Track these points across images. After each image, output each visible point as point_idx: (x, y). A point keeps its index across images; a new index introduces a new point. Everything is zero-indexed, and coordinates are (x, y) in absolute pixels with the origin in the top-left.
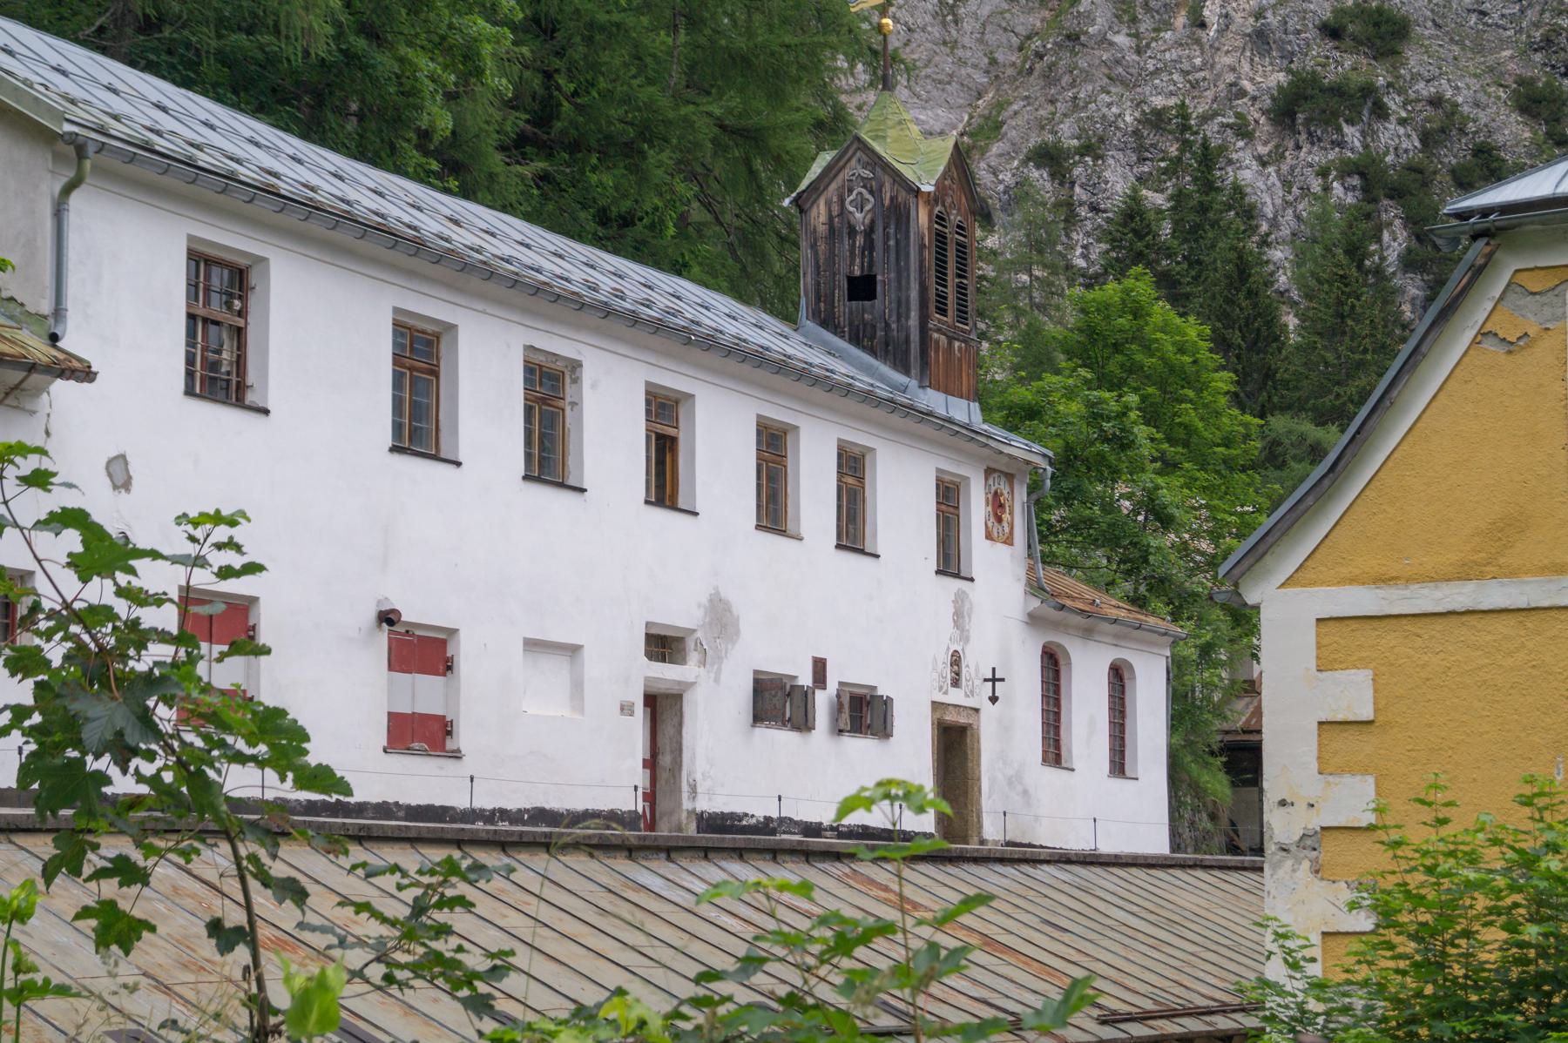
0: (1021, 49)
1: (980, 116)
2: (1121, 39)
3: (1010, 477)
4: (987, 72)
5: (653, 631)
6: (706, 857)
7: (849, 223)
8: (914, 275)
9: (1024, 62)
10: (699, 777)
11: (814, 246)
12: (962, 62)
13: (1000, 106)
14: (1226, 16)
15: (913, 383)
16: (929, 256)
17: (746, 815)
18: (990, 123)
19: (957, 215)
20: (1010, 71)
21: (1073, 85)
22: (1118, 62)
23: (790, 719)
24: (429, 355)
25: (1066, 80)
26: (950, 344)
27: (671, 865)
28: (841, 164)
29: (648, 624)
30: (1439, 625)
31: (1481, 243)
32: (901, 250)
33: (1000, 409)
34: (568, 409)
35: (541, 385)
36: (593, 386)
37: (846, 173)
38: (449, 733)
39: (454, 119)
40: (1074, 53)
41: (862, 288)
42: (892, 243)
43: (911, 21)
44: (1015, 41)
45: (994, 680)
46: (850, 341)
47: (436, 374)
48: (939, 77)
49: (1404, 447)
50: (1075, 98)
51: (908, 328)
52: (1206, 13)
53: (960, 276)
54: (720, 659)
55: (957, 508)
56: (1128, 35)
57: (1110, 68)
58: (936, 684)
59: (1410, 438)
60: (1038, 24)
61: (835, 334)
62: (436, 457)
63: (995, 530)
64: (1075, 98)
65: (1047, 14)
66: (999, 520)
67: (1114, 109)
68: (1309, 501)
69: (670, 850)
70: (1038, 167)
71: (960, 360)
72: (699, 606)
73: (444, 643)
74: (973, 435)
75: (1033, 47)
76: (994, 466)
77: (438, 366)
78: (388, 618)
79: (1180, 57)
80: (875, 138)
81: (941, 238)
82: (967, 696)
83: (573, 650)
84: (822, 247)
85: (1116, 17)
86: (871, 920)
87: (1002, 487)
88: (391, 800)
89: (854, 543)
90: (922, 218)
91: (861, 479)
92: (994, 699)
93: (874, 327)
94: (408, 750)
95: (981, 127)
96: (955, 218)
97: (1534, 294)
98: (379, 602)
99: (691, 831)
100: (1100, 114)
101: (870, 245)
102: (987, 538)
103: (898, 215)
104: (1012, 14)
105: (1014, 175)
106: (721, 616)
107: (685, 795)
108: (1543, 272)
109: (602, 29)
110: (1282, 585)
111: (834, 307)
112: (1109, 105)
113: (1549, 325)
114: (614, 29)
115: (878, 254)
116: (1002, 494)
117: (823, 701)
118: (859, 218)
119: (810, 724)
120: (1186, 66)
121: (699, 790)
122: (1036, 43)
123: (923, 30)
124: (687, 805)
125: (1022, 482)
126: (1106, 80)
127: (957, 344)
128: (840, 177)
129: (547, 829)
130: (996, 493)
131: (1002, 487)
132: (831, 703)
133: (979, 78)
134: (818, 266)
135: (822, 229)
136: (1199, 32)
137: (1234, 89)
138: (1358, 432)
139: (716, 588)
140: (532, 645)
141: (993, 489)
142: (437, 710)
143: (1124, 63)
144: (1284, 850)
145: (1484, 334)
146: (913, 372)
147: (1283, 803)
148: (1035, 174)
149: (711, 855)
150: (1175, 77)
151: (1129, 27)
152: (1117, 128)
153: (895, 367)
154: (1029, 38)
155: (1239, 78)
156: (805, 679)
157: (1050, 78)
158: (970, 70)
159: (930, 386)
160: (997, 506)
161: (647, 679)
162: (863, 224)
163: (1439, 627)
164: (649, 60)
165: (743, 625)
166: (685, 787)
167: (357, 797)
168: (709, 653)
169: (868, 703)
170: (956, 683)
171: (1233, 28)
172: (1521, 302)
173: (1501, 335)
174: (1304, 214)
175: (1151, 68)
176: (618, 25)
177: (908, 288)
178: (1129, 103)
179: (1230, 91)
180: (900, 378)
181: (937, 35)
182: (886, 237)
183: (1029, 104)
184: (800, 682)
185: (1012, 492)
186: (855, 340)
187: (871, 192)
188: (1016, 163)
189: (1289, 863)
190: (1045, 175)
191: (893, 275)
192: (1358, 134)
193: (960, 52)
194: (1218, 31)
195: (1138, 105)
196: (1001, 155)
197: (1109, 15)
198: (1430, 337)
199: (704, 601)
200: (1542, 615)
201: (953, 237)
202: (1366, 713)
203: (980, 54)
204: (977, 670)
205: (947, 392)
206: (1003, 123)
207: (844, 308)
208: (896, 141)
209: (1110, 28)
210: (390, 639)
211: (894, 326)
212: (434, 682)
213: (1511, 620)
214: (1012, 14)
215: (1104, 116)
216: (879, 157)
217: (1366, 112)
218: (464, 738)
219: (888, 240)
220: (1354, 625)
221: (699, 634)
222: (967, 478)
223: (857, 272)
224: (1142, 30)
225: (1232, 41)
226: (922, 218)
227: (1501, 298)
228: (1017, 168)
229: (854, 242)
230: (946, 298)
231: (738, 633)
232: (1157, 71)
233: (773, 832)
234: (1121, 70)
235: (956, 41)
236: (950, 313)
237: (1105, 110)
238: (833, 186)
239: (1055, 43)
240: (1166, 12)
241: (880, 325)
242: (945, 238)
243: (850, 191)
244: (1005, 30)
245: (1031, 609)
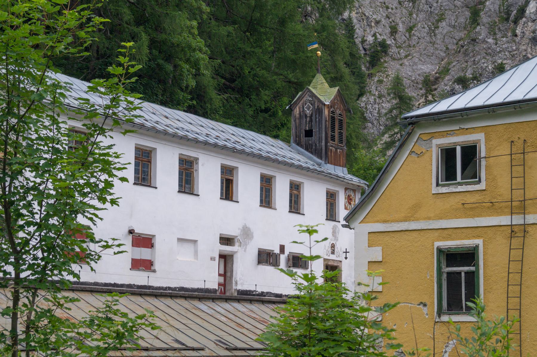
0: (457, 44)
1: (442, 67)
2: (490, 40)
3: (354, 191)
4: (445, 52)
6: (226, 301)
9: (458, 48)
10: (238, 279)
11: (295, 121)
12: (437, 49)
13: (449, 63)
14: (523, 32)
15: (323, 162)
16: (329, 124)
18: (445, 69)
20: (453, 52)
21: (473, 56)
22: (489, 48)
24: (148, 157)
25: (471, 54)
26: (336, 150)
27: (213, 303)
28: (303, 96)
29: (220, 234)
30: (399, 234)
31: (411, 126)
32: (320, 121)
33: (375, 169)
34: (194, 172)
35: (185, 164)
36: (203, 165)
37: (305, 99)
38: (152, 265)
39: (196, 82)
40: (474, 45)
41: (309, 133)
42: (317, 120)
43: (419, 35)
44: (455, 41)
45: (346, 252)
46: (305, 150)
47: (150, 162)
48: (429, 54)
49: (391, 184)
50: (474, 60)
51: (322, 146)
52: (517, 31)
55: (335, 200)
56: (493, 39)
57: (486, 50)
59: (393, 181)
60: (463, 36)
61: (301, 147)
62: (150, 186)
64: (474, 60)
65: (466, 32)
66: (350, 204)
67: (485, 65)
68: (366, 199)
69: (227, 300)
70: (458, 84)
72: (239, 229)
73: (151, 239)
74: (339, 178)
75: (460, 43)
77: (151, 160)
78: (131, 232)
79: (508, 47)
80: (314, 88)
81: (333, 118)
82: (337, 257)
83: (195, 242)
85: (489, 33)
87: (351, 193)
88: (132, 284)
89: (298, 211)
90: (326, 112)
91: (299, 192)
92: (346, 258)
93: (312, 145)
94: (138, 269)
95: (442, 71)
96: (338, 112)
97: (425, 140)
98: (129, 227)
99: (236, 294)
100: (480, 66)
101: (311, 121)
102: (345, 209)
103: (319, 111)
104: (454, 32)
105: (450, 87)
106: (247, 232)
107: (234, 285)
108: (427, 134)
109: (248, 53)
112: (484, 63)
113: (428, 150)
114: (252, 53)
115: (313, 123)
116: (351, 196)
117: (283, 259)
118: (308, 112)
120: (510, 49)
121: (238, 283)
122: (461, 43)
123: (424, 38)
124: (234, 287)
125: (359, 192)
126: (485, 54)
127: (339, 150)
128: (303, 99)
129: (183, 292)
130: (349, 195)
131: (351, 193)
132: (286, 257)
133: (443, 54)
134: (296, 127)
135: (297, 116)
136: (515, 38)
137: (525, 57)
138: (379, 179)
140: (180, 240)
141: (348, 194)
142: (149, 258)
143: (491, 48)
145: (412, 152)
146: (323, 159)
148: (457, 87)
149: (252, 302)
150: (506, 53)
151: (493, 36)
152: (486, 71)
153: (318, 157)
154: (460, 40)
155: (527, 53)
156: (277, 251)
157: (466, 54)
158: (439, 52)
159: (328, 163)
161: (220, 250)
163: (399, 235)
164: (263, 62)
165: (254, 235)
166: (234, 282)
167: (81, 280)
170: (333, 253)
171: (525, 37)
172: (422, 143)
173: (416, 152)
175: (498, 50)
176: (253, 52)
177: (322, 134)
178: (490, 62)
179: (524, 58)
180: (319, 161)
181: (428, 40)
183: (459, 63)
184: (275, 252)
186: (307, 149)
187: (312, 105)
188: (451, 83)
190: (460, 87)
191: (317, 130)
193: (436, 46)
194: (520, 38)
195: (493, 63)
196: (449, 80)
197: (486, 32)
198: (397, 153)
199: (241, 227)
200: (425, 231)
201: (337, 117)
202: (380, 259)
203: (443, 46)
204: (341, 249)
205: (335, 165)
206: (450, 69)
207: (304, 139)
208: (320, 89)
209: (486, 37)
210: (133, 238)
211: (318, 145)
212: (149, 250)
213: (417, 233)
214: (454, 32)
215: (482, 67)
216: (314, 94)
218: (157, 266)
220: (378, 234)
221: (239, 237)
222: (338, 191)
223: (307, 129)
224: (498, 37)
225: (525, 41)
226: (326, 112)
227: (416, 142)
228: (451, 85)
230: (335, 136)
231: (253, 237)
232: (500, 52)
233: (265, 296)
234: (490, 51)
235: (435, 42)
236: (336, 141)
237: (482, 65)
238: (301, 103)
239: (468, 42)
240: (506, 31)
241: (314, 145)
243: (306, 104)
244: (452, 38)
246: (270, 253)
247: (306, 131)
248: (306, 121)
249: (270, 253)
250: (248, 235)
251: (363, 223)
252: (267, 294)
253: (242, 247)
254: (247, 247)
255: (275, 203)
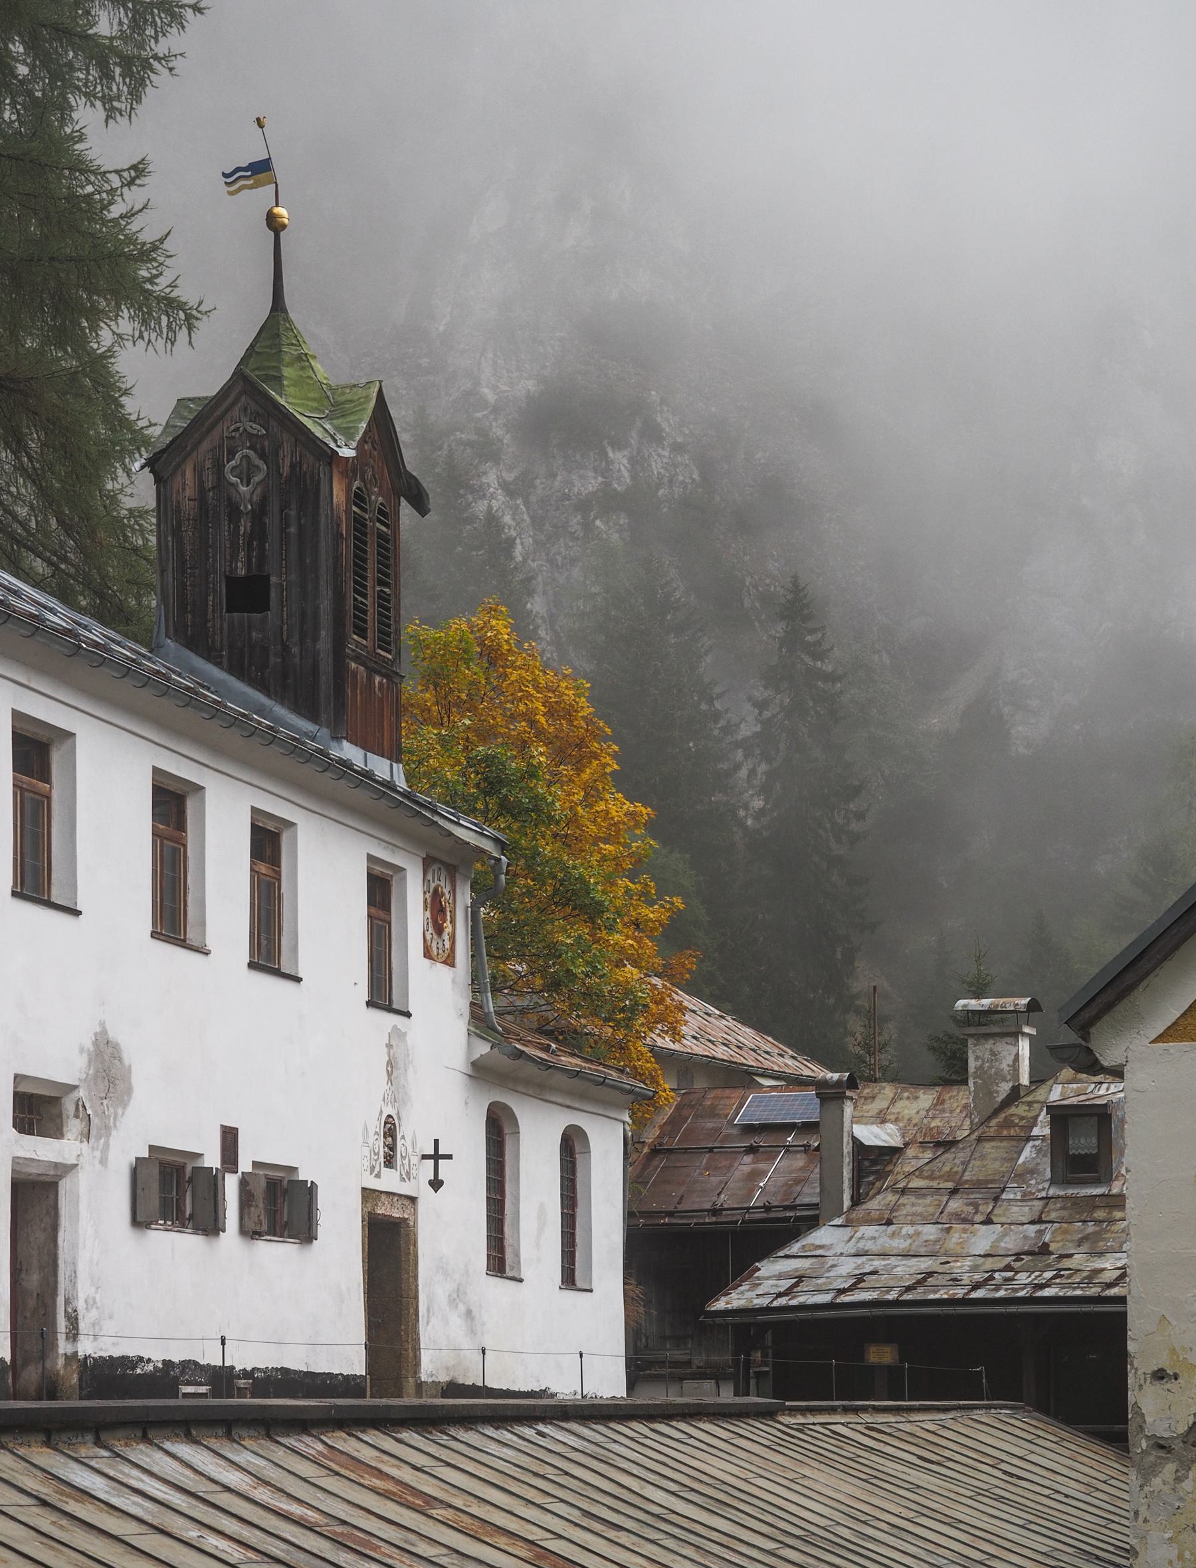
5: (24, 1088)
7: (229, 499)
8: (325, 578)
10: (80, 1305)
15: (325, 732)
16: (347, 549)
17: (141, 1359)
19: (379, 495)
23: (191, 1217)
28: (218, 413)
42: (293, 530)
45: (436, 1157)
46: (230, 671)
53: (381, 583)
54: (107, 1130)
58: (367, 1164)
61: (208, 659)
63: (434, 945)
66: (439, 930)
71: (381, 701)
72: (82, 1050)
76: (434, 853)
81: (359, 524)
82: (403, 1180)
84: (188, 534)
86: (61, 1446)
87: (442, 883)
92: (436, 1184)
110: (1160, 1039)
111: (207, 621)
116: (443, 894)
119: (220, 1226)
124: (63, 1347)
125: (466, 877)
127: (377, 679)
128: (217, 431)
130: (436, 891)
139: (102, 1024)
141: (433, 886)
144: (1162, 1447)
146: (323, 717)
147: (1160, 1375)
153: (297, 709)
156: (212, 1160)
160: (437, 910)
162: (250, 501)
165: (136, 1079)
166: (62, 1324)
168: (95, 1121)
169: (285, 1192)
170: (390, 1162)
174: (559, 558)
182: (285, 522)
185: (453, 892)
187: (262, 456)
189: (1170, 1468)
191: (293, 577)
192: (625, 461)
199: (88, 1044)
211: (295, 650)
217: (634, 434)
219: (288, 526)
221: (82, 1093)
223: (242, 572)
229: (237, 528)
231: (129, 1090)
236: (370, 634)
238: (206, 445)
242: (365, 526)
243: (232, 454)
245: (476, 1056)
246: (180, 1169)
247: (232, 582)
248: (235, 534)
249: (180, 1169)
250: (112, 1082)
251: (1181, 1038)
252: (183, 1372)
253: (92, 1140)
254: (112, 1141)
255: (202, 924)
